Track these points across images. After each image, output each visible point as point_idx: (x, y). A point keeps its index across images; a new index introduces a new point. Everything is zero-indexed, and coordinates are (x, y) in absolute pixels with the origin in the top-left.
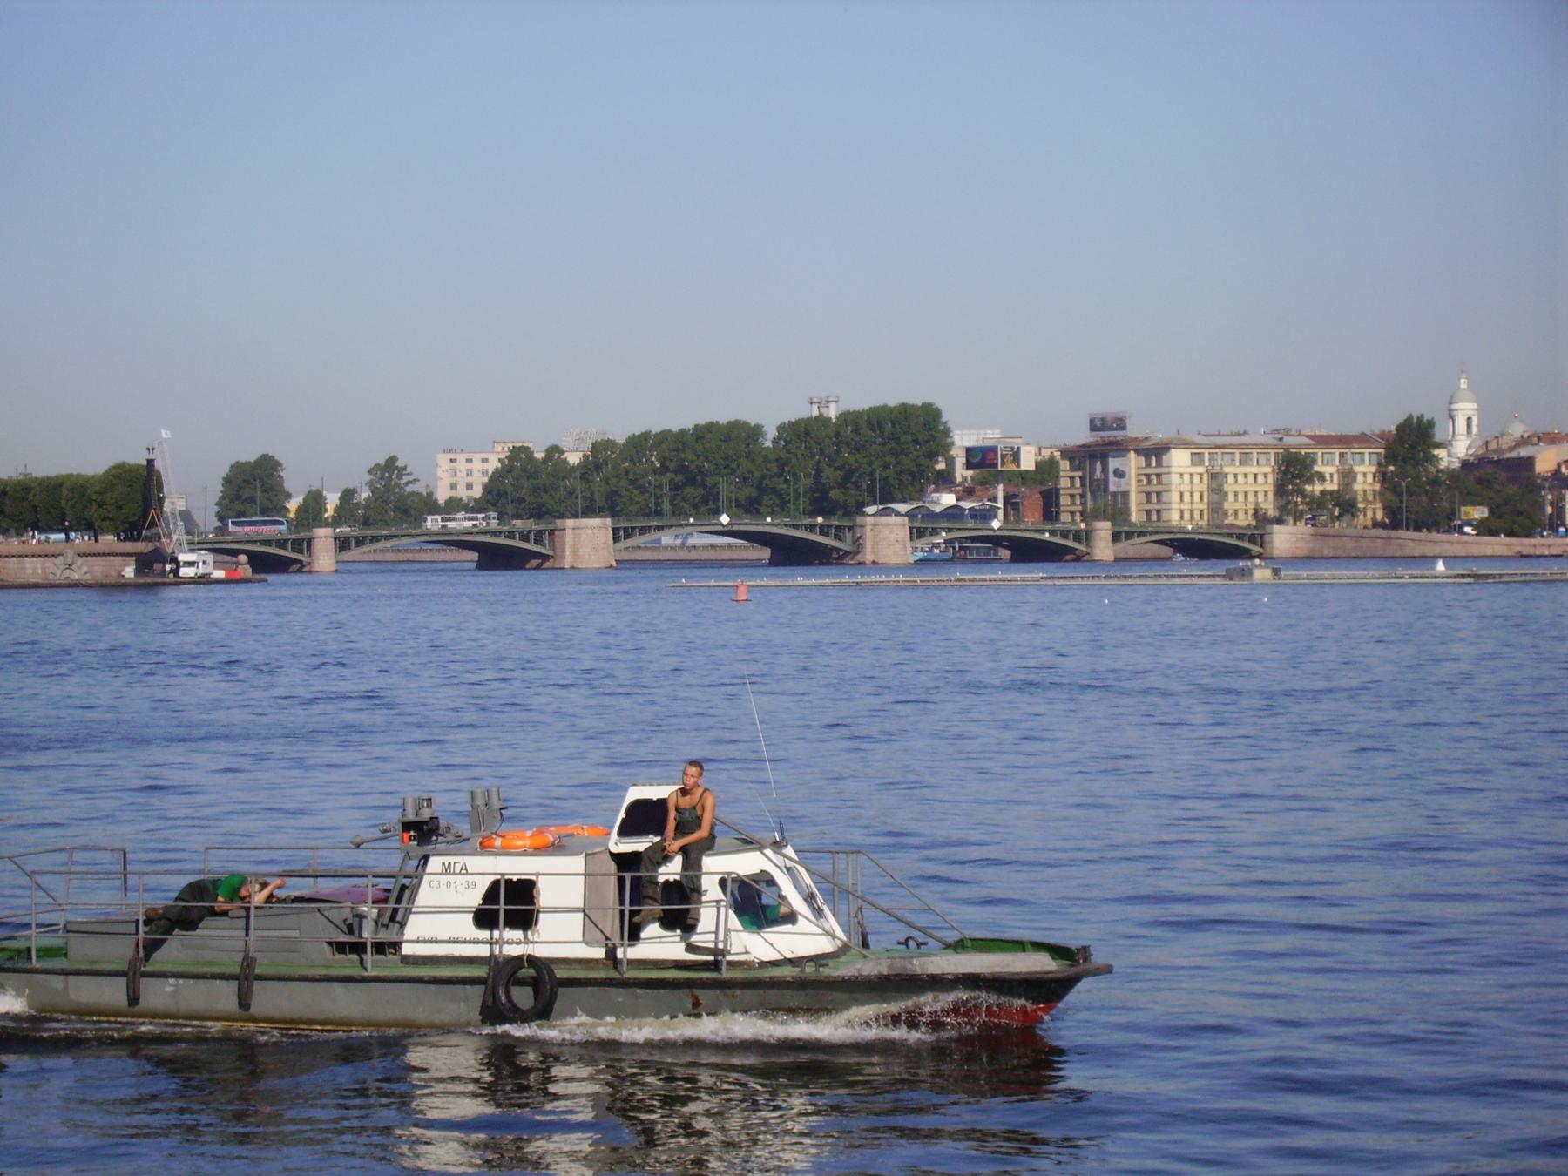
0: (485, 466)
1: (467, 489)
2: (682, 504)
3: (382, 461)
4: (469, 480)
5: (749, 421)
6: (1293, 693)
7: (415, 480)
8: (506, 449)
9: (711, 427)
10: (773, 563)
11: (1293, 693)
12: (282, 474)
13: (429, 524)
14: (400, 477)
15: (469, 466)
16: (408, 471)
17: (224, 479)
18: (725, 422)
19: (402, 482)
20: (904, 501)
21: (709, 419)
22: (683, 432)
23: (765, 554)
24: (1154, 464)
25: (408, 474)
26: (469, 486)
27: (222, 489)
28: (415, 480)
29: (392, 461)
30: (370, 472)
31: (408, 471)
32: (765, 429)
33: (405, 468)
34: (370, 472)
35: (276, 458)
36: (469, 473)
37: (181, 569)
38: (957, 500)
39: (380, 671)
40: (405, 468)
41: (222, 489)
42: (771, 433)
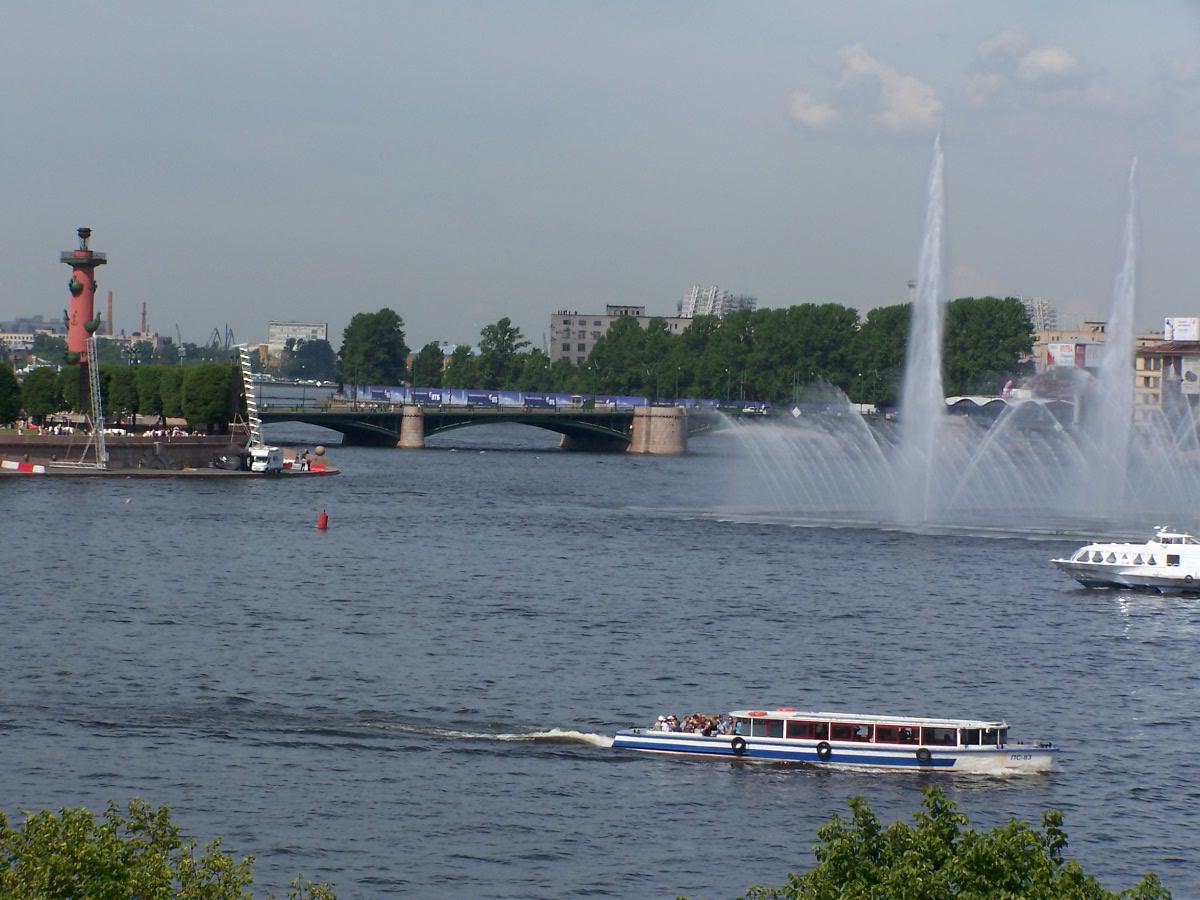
0: (597, 329)
1: (564, 349)
2: (717, 379)
3: (495, 323)
4: (582, 341)
5: (782, 307)
6: (887, 805)
7: (527, 343)
8: (619, 313)
9: (807, 309)
10: (567, 450)
11: (887, 805)
12: (401, 329)
13: (596, 405)
14: (512, 338)
15: (582, 328)
16: (521, 333)
17: (346, 330)
18: (820, 305)
19: (514, 344)
20: (984, 394)
21: (805, 301)
22: (780, 312)
23: (560, 439)
24: (1152, 368)
25: (520, 337)
26: (582, 347)
27: (344, 339)
28: (527, 343)
29: (505, 323)
30: (483, 333)
31: (521, 333)
32: (858, 314)
33: (517, 330)
34: (483, 333)
35: (397, 313)
36: (582, 334)
37: (254, 464)
38: (1033, 397)
39: (387, 869)
40: (517, 330)
41: (344, 339)
42: (864, 319)
